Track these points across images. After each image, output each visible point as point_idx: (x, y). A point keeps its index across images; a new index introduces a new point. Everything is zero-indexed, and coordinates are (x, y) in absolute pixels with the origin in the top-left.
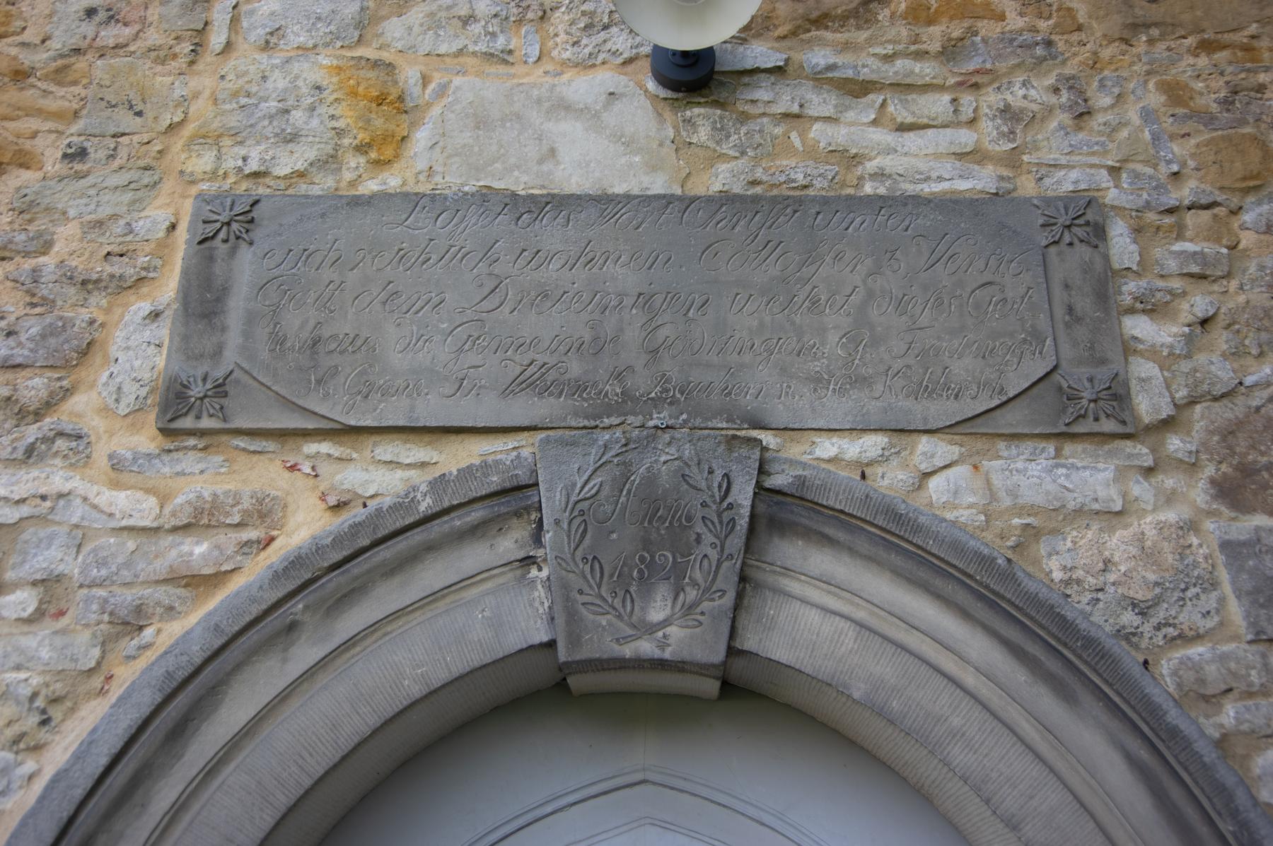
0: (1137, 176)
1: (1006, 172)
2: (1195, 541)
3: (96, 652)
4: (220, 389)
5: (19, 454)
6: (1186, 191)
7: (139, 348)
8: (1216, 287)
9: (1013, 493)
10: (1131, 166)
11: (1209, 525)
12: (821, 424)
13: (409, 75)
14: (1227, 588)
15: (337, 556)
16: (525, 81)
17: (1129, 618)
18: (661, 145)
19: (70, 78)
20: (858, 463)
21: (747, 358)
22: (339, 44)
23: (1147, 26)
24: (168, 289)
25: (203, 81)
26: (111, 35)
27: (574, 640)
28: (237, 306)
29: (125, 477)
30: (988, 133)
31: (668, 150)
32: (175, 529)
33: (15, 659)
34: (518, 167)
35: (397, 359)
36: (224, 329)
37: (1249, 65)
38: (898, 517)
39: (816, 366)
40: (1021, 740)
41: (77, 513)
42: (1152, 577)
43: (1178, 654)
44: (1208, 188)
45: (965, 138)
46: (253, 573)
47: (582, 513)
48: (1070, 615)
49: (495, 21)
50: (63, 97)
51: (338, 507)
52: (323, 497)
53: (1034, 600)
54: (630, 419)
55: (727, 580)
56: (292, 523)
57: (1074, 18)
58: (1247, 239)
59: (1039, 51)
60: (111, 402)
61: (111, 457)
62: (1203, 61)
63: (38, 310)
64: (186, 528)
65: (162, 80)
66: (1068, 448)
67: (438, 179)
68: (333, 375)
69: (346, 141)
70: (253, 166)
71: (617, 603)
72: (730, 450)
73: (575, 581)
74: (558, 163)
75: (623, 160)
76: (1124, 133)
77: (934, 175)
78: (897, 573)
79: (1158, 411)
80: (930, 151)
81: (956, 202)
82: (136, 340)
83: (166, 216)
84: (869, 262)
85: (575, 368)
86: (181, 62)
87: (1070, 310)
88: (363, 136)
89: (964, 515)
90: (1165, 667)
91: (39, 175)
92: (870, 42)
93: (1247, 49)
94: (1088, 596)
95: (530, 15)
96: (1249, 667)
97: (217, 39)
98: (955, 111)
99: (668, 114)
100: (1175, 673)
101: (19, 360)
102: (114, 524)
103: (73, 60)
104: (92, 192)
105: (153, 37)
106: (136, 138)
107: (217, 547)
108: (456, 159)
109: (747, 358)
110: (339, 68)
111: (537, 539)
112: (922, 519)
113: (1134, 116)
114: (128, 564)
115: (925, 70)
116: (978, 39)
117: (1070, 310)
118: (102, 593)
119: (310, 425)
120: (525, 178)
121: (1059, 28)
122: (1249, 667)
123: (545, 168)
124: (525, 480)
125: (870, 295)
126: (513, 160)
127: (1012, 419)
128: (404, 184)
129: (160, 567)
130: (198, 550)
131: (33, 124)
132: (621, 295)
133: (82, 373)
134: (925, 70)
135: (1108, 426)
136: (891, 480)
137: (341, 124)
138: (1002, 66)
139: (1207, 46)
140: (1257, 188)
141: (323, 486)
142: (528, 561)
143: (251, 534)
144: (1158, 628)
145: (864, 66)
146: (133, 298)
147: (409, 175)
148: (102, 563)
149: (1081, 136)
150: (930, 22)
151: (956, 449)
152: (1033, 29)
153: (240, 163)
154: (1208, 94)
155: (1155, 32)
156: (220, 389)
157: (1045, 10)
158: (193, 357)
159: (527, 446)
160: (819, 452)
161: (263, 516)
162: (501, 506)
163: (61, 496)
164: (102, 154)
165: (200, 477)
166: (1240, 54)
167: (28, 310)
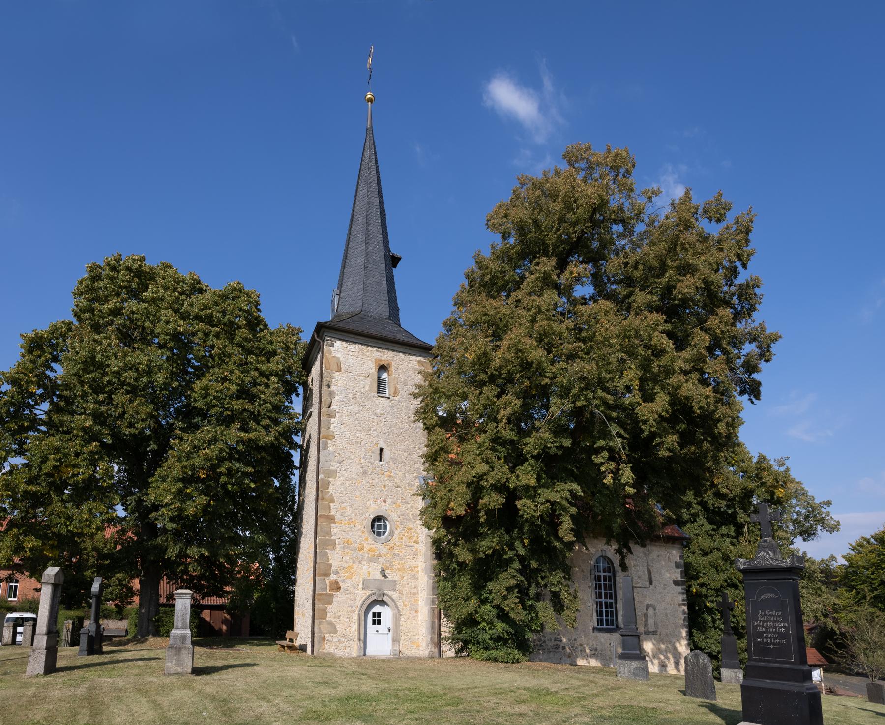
7: (361, 586)
83: (361, 579)
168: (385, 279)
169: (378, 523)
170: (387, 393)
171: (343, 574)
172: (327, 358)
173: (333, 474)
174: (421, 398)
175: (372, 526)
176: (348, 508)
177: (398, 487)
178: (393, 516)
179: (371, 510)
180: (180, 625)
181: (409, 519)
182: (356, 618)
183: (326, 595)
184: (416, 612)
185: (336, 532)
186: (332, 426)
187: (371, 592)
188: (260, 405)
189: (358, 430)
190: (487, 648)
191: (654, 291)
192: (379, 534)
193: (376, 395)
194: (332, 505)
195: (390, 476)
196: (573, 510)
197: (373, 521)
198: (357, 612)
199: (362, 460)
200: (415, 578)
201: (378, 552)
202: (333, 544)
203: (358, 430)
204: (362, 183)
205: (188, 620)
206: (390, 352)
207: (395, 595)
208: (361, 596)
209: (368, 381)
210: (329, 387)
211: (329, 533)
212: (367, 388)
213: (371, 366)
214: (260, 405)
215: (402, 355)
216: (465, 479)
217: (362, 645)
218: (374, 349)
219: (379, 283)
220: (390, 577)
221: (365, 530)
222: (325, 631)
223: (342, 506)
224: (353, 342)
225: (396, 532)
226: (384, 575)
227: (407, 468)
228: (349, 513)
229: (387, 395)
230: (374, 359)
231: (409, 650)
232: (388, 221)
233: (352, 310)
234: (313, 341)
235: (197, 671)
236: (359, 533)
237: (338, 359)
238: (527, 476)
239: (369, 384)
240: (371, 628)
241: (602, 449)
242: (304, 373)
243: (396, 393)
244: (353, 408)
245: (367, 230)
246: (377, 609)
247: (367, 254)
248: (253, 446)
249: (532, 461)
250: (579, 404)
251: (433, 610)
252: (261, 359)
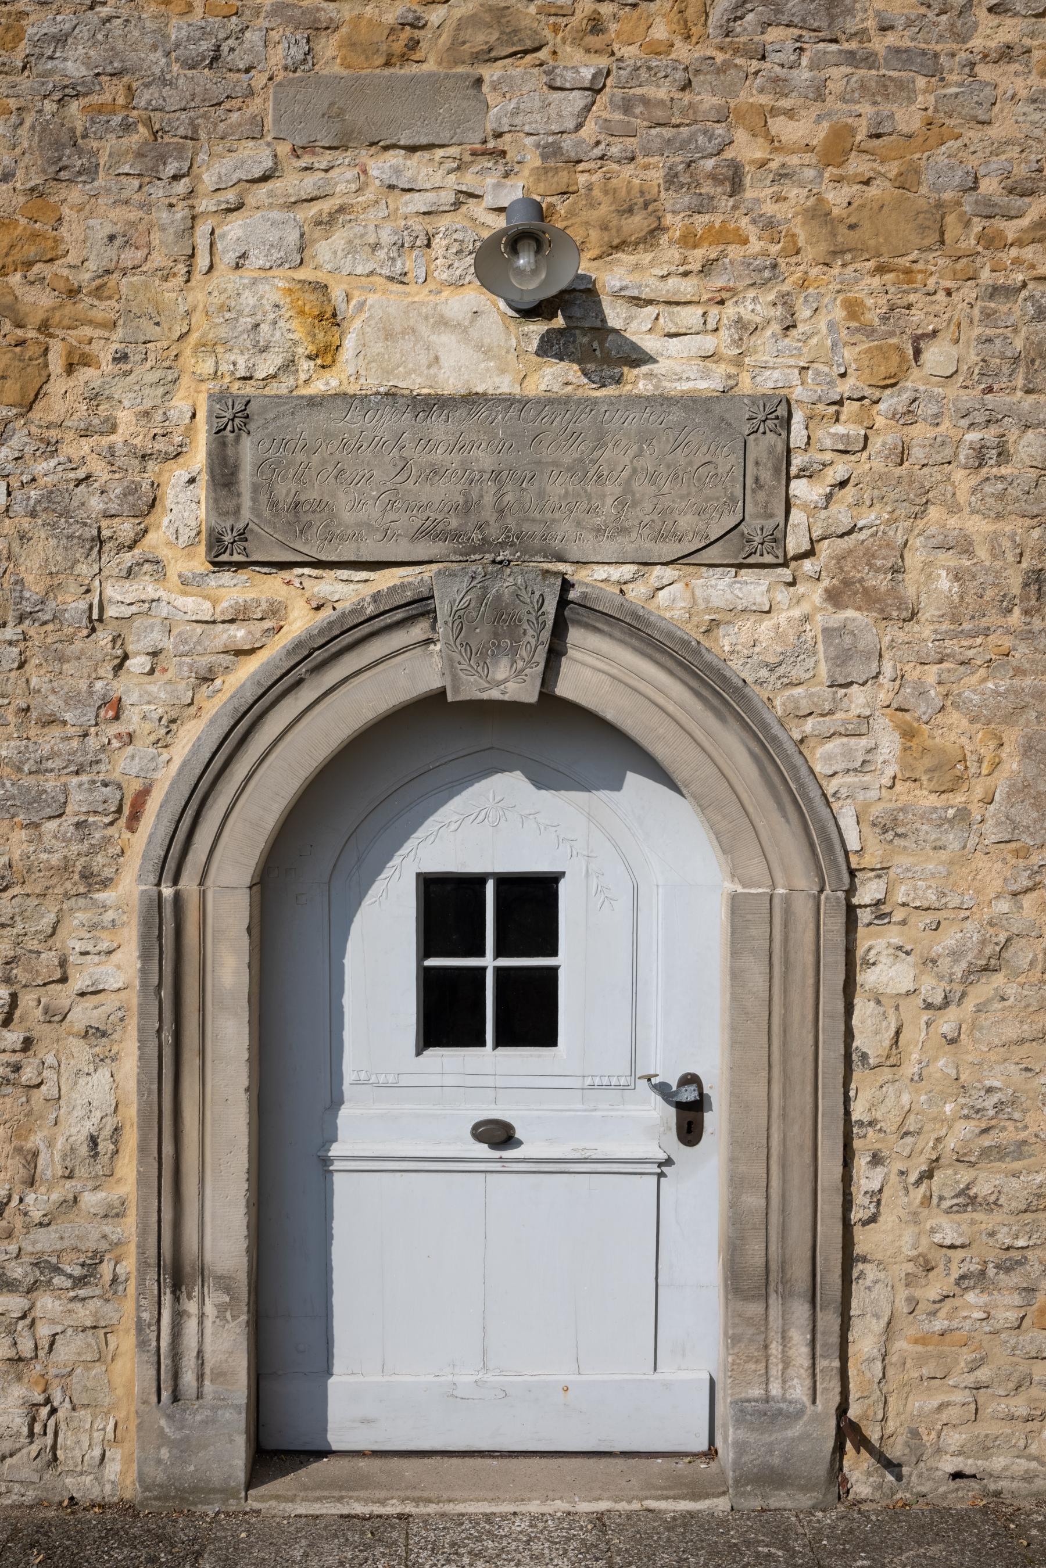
0: (818, 373)
1: (733, 370)
2: (808, 628)
3: (190, 693)
4: (243, 536)
5: (124, 573)
6: (847, 387)
7: (186, 505)
8: (853, 458)
9: (707, 600)
10: (815, 365)
11: (818, 618)
12: (599, 559)
13: (337, 294)
14: (821, 655)
15: (321, 641)
16: (416, 299)
17: (764, 673)
18: (508, 352)
19: (105, 294)
20: (619, 582)
21: (557, 515)
22: (287, 266)
23: (843, 252)
24: (198, 458)
25: (197, 296)
26: (130, 257)
27: (456, 690)
28: (246, 477)
29: (188, 588)
30: (723, 342)
31: (512, 356)
32: (224, 622)
33: (146, 698)
34: (414, 371)
35: (347, 516)
36: (239, 495)
37: (905, 286)
38: (638, 617)
39: (599, 520)
40: (695, 741)
41: (164, 610)
42: (779, 649)
43: (787, 693)
44: (860, 384)
45: (709, 343)
46: (275, 649)
47: (460, 617)
48: (728, 674)
49: (395, 248)
50: (103, 310)
51: (318, 608)
52: (308, 601)
53: (709, 666)
54: (487, 556)
55: (541, 656)
56: (291, 618)
57: (795, 243)
58: (880, 422)
59: (767, 274)
60: (173, 539)
61: (180, 576)
62: (876, 282)
63: (117, 476)
64: (232, 621)
65: (168, 292)
66: (743, 571)
67: (362, 381)
68: (309, 528)
69: (300, 350)
70: (242, 372)
71: (480, 669)
72: (544, 579)
73: (457, 657)
74: (440, 368)
75: (483, 365)
76: (814, 341)
77: (685, 376)
78: (635, 649)
79: (800, 547)
80: (685, 355)
81: (694, 400)
82: (182, 497)
83: (190, 404)
84: (635, 447)
85: (454, 523)
86: (180, 279)
87: (757, 480)
88: (312, 349)
89: (677, 614)
90: (778, 702)
91: (98, 372)
92: (652, 264)
93: (908, 272)
94: (742, 660)
95: (418, 243)
96: (825, 700)
97: (202, 261)
98: (705, 323)
99: (512, 328)
100: (783, 704)
101: (113, 512)
102: (187, 617)
103: (105, 279)
104: (137, 388)
105: (158, 259)
106: (159, 344)
107: (250, 632)
108: (374, 364)
109: (557, 515)
110: (290, 290)
111: (433, 628)
112: (652, 618)
113: (823, 327)
114: (199, 642)
115: (687, 287)
116: (727, 260)
117: (757, 480)
118: (187, 659)
119: (299, 558)
120: (419, 380)
121: (784, 253)
122: (825, 700)
123: (432, 371)
124: (426, 594)
125: (634, 471)
126: (410, 366)
127: (712, 555)
128: (341, 384)
129: (219, 644)
130: (239, 634)
131: (87, 331)
132: (482, 472)
133: (151, 519)
134: (687, 287)
135: (768, 559)
136: (637, 592)
137: (295, 336)
138: (740, 285)
139: (881, 270)
140: (893, 385)
141: (308, 594)
142: (429, 641)
143: (267, 624)
144: (779, 678)
145: (647, 286)
146: (175, 466)
147: (344, 378)
148: (185, 642)
149: (787, 340)
150: (695, 246)
151: (677, 573)
152: (765, 254)
153: (232, 368)
154: (874, 311)
155: (848, 257)
156: (243, 536)
157: (776, 236)
158: (223, 514)
159: (428, 572)
160: (596, 577)
161: (274, 613)
162: (412, 610)
163: (153, 601)
164: (138, 357)
165: (235, 589)
166: (902, 277)
167: (111, 476)
182: (119, 969)
187: (347, 592)
198: (129, 887)
207: (760, 620)
220: (679, 360)
226: (572, 322)
240: (396, 1089)
246: (489, 825)
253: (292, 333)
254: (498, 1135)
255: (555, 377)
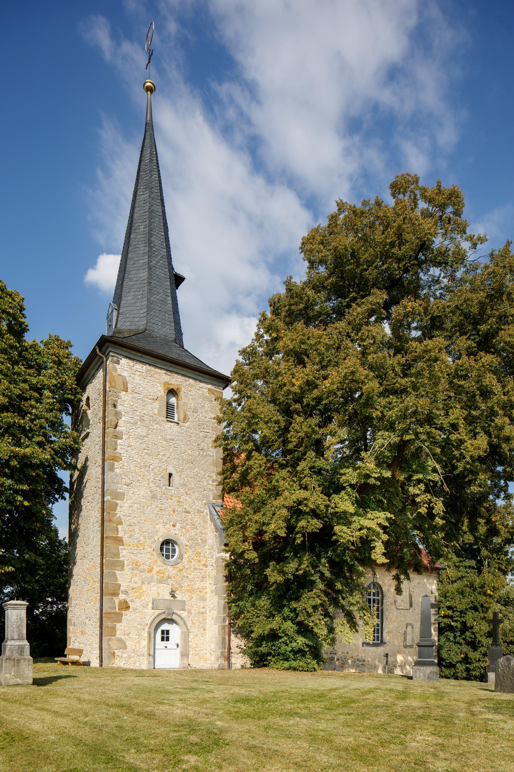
7: (150, 605)
165: (153, 611)
168: (170, 298)
169: (167, 545)
170: (176, 416)
171: (131, 594)
172: (112, 376)
173: (121, 496)
174: (225, 424)
175: (162, 549)
176: (137, 531)
177: (188, 512)
178: (182, 540)
179: (160, 534)
180: (16, 637)
181: (198, 544)
182: (146, 635)
183: (115, 613)
184: (204, 630)
185: (124, 553)
186: (119, 447)
187: (160, 611)
188: (32, 421)
189: (147, 454)
190: (287, 660)
191: (472, 337)
192: (167, 557)
193: (165, 419)
194: (120, 527)
195: (179, 502)
196: (385, 537)
197: (162, 544)
198: (147, 630)
199: (151, 485)
200: (204, 599)
201: (167, 574)
202: (121, 565)
203: (147, 454)
204: (142, 187)
205: (25, 632)
206: (179, 377)
207: (184, 614)
208: (150, 615)
209: (156, 404)
210: (115, 406)
211: (117, 555)
212: (156, 411)
213: (160, 388)
214: (32, 421)
215: (191, 381)
216: (287, 504)
217: (151, 659)
218: (163, 371)
219: (164, 302)
220: (179, 597)
221: (154, 553)
222: (115, 648)
223: (131, 528)
224: (141, 362)
225: (186, 556)
226: (173, 596)
227: (197, 495)
228: (138, 536)
229: (176, 420)
230: (162, 381)
231: (197, 663)
232: (170, 233)
233: (133, 327)
234: (93, 355)
235: (38, 682)
236: (149, 556)
237: (124, 378)
238: (344, 503)
239: (157, 408)
241: (419, 481)
242: (79, 390)
243: (185, 419)
244: (142, 431)
245: (150, 242)
246: (165, 627)
247: (150, 268)
248: (26, 462)
249: (349, 490)
250: (407, 437)
251: (224, 628)
252: (31, 371)
253: (156, 595)
254: (166, 647)
255: (172, 598)
